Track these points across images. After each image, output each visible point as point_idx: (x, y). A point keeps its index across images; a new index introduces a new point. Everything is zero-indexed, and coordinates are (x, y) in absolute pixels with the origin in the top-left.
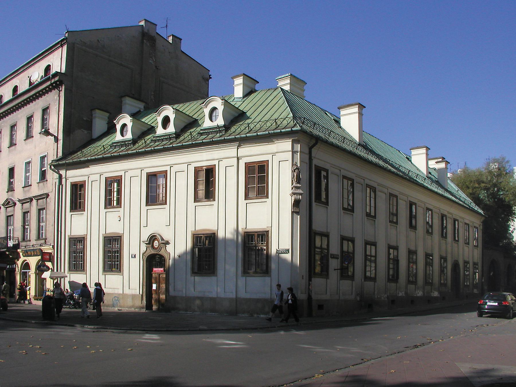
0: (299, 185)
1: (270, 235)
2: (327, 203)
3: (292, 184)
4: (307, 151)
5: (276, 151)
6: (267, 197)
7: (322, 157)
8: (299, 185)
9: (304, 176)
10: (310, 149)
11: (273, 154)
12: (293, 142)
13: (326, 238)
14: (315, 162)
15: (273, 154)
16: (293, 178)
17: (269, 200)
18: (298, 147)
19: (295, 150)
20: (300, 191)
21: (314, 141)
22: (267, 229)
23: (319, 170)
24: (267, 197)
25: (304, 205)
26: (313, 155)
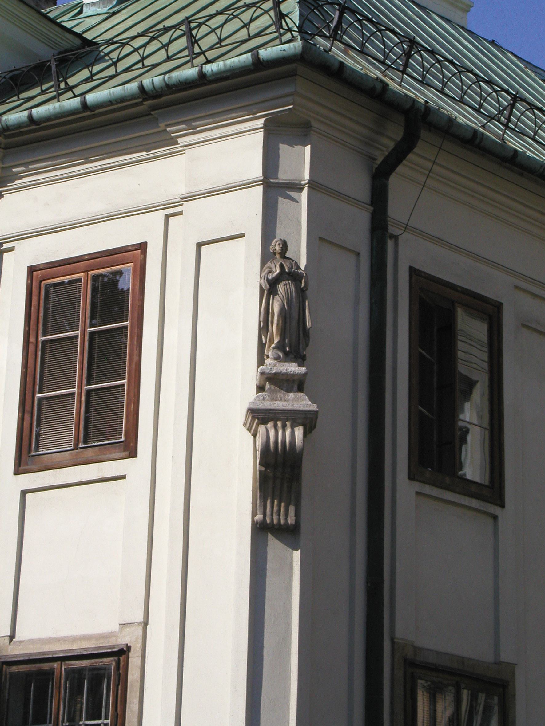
0: (292, 368)
1: (133, 675)
2: (493, 491)
3: (261, 361)
4: (359, 186)
5: (182, 190)
6: (130, 450)
7: (449, 229)
8: (292, 368)
9: (339, 321)
10: (380, 177)
11: (171, 210)
12: (277, 134)
13: (28, 495)
14: (410, 253)
15: (171, 210)
16: (264, 328)
17: (136, 468)
18: (299, 161)
19: (284, 175)
20: (301, 402)
21: (395, 133)
22: (122, 640)
23: (438, 310)
24: (130, 450)
25: (334, 481)
26: (397, 210)
